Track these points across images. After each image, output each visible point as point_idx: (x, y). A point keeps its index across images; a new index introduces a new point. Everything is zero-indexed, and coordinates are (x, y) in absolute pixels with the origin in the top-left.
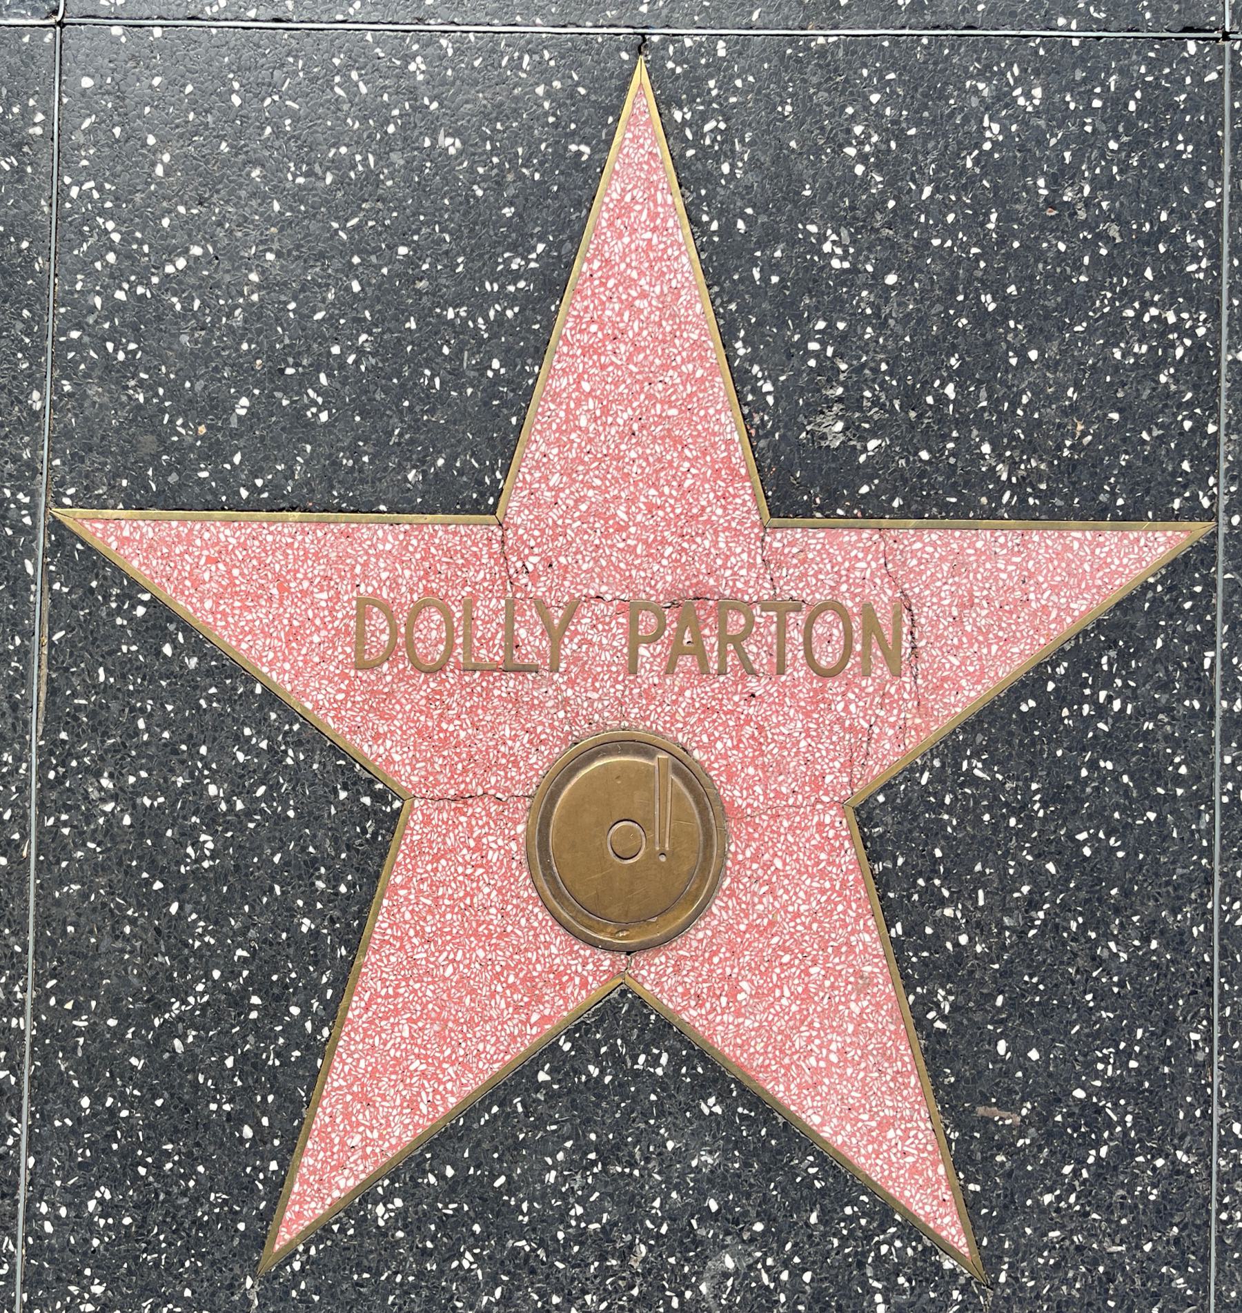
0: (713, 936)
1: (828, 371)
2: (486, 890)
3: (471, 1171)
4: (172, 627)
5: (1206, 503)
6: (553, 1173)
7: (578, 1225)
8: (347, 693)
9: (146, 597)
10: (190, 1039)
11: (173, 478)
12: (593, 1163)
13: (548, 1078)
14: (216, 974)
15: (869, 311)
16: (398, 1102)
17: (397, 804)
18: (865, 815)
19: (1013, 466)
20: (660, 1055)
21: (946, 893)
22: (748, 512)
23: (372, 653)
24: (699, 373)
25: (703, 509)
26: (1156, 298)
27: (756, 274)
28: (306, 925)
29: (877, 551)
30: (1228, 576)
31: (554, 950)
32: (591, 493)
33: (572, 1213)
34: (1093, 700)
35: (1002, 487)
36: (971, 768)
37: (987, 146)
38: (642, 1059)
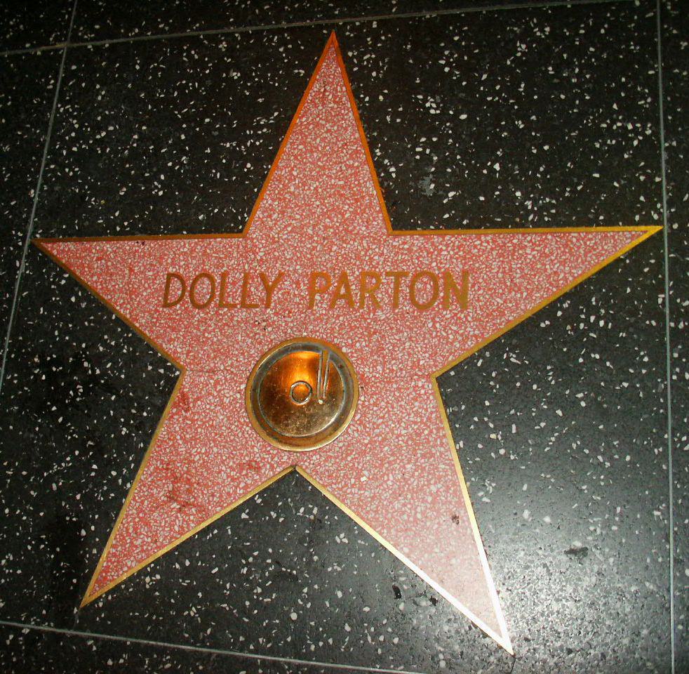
0: (349, 446)
1: (426, 159)
2: (222, 417)
3: (200, 564)
4: (76, 289)
5: (656, 217)
6: (246, 569)
7: (258, 598)
8: (157, 319)
9: (67, 276)
10: (61, 484)
11: (87, 223)
12: (270, 565)
13: (247, 517)
14: (77, 453)
15: (450, 132)
16: (163, 524)
17: (177, 373)
18: (443, 381)
19: (535, 202)
20: (312, 509)
21: (491, 425)
22: (380, 228)
23: (172, 299)
24: (356, 164)
25: (355, 228)
26: (620, 118)
27: (388, 118)
28: (124, 431)
29: (454, 246)
30: (672, 255)
31: (256, 450)
32: (294, 222)
33: (255, 591)
34: (587, 321)
35: (528, 212)
36: (508, 358)
37: (519, 54)
38: (302, 510)
